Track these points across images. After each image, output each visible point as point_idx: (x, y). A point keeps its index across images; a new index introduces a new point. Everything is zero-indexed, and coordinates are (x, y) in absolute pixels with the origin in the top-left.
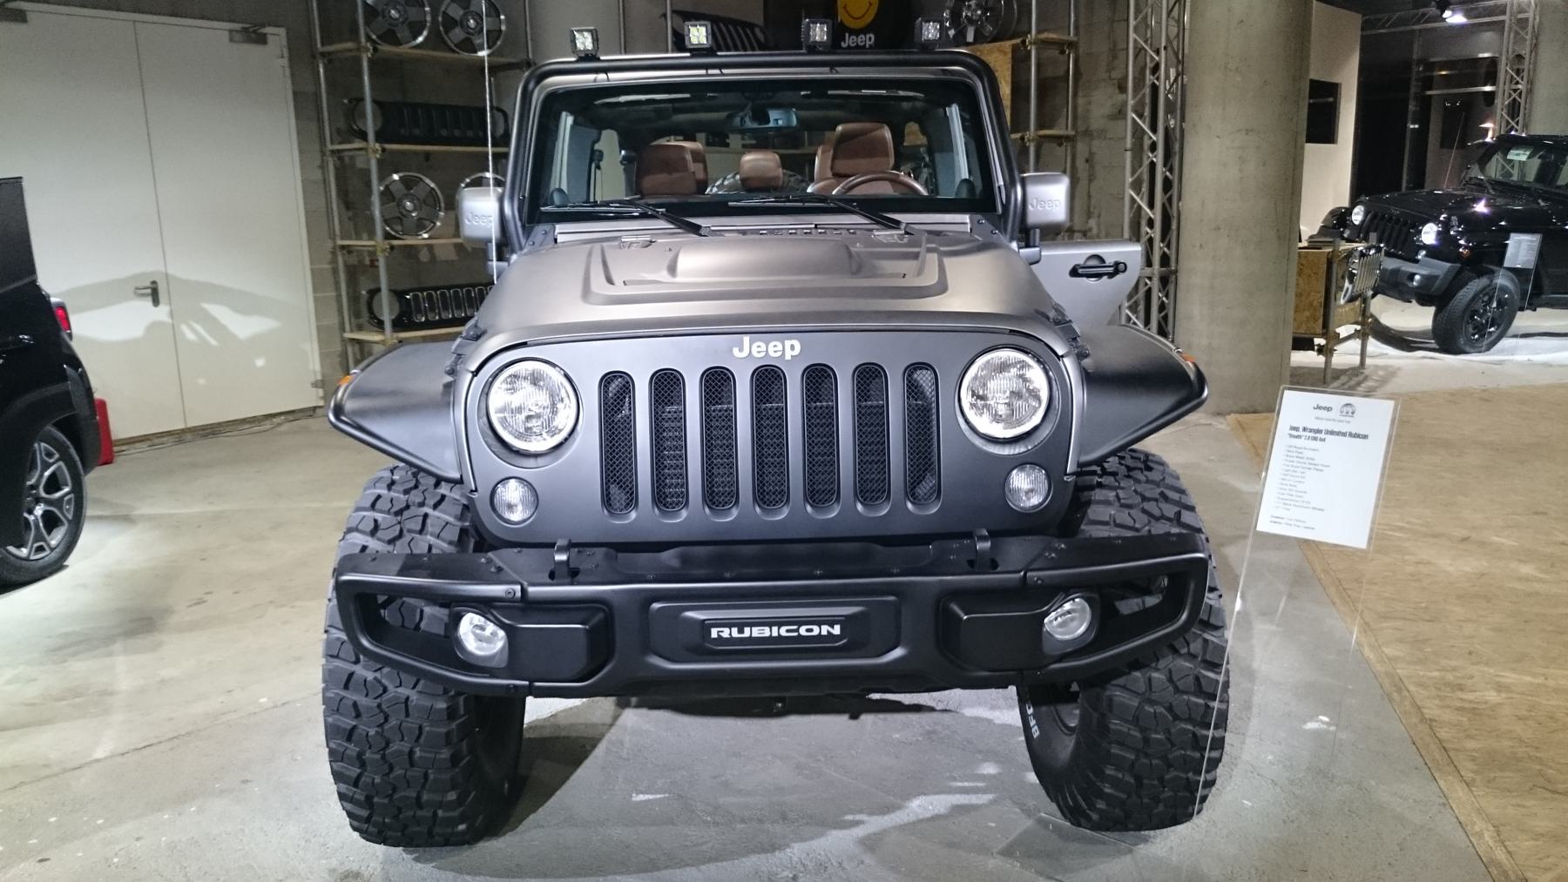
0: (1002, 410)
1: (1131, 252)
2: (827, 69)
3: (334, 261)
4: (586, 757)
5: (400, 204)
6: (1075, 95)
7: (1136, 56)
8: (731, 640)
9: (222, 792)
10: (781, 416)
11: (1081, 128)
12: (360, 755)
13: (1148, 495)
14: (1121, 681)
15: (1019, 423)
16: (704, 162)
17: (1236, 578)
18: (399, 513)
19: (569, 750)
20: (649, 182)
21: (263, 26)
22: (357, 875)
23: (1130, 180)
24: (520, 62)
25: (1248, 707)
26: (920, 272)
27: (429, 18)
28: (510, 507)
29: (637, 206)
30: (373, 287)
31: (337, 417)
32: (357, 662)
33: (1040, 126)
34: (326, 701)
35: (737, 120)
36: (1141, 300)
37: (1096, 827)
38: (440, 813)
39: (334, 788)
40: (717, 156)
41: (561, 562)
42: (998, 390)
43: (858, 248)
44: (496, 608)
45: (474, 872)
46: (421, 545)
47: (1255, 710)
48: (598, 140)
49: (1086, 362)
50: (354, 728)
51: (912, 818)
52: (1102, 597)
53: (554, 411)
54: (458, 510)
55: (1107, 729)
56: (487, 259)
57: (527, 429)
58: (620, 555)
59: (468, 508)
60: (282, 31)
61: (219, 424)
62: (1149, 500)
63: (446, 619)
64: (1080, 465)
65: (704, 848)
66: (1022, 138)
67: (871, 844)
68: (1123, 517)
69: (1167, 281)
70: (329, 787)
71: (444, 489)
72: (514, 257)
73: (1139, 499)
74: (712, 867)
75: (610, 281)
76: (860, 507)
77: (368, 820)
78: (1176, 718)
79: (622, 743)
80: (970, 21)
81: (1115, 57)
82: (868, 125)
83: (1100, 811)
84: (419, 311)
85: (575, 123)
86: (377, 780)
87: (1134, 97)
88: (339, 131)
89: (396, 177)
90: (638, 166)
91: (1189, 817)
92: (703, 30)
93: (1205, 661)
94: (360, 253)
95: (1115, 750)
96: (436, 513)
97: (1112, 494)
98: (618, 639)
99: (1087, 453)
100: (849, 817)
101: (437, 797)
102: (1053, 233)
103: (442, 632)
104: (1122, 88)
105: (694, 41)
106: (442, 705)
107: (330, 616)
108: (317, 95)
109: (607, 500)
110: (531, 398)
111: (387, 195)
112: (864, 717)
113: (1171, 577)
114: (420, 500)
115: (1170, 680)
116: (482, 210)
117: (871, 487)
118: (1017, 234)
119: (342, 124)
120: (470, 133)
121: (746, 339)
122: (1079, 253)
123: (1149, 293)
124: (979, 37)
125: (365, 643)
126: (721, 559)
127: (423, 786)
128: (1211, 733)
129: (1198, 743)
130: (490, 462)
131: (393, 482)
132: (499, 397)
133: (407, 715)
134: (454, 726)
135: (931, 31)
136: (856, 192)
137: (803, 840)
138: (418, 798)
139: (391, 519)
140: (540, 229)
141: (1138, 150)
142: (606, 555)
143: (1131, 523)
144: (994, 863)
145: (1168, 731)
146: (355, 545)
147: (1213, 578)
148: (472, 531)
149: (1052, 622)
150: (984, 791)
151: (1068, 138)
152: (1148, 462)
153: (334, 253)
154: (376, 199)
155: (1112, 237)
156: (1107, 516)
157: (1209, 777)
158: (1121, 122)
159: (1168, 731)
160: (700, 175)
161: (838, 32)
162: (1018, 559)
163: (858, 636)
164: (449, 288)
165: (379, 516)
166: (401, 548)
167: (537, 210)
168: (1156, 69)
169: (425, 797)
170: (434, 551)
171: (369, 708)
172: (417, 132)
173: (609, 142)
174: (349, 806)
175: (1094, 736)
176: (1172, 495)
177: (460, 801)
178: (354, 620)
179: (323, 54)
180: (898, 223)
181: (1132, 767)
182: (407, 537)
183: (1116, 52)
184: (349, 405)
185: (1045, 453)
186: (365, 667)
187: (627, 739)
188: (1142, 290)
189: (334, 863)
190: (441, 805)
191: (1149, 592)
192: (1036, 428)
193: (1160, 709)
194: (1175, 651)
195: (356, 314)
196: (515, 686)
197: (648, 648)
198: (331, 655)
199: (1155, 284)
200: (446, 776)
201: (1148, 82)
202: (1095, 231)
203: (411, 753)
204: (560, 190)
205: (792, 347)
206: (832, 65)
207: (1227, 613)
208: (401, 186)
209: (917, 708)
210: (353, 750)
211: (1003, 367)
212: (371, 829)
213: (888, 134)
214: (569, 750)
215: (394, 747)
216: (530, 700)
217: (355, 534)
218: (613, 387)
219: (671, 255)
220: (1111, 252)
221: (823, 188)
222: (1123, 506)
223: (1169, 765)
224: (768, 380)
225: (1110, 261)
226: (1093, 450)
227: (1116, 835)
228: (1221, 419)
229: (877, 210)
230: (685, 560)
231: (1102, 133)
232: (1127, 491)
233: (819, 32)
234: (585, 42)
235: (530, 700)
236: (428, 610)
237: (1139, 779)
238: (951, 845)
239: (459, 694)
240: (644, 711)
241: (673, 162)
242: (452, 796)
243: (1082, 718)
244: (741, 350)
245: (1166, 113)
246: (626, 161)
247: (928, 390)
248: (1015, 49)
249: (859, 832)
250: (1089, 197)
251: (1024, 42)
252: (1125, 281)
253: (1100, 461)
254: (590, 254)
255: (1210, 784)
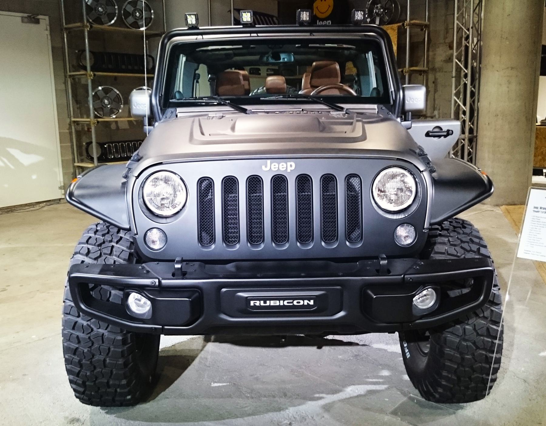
0: (393, 197)
1: (455, 125)
2: (309, 34)
3: (70, 128)
4: (190, 365)
5: (102, 101)
6: (428, 51)
7: (458, 32)
8: (260, 307)
9: (13, 380)
10: (285, 199)
11: (431, 66)
12: (80, 361)
13: (464, 239)
14: (450, 330)
15: (402, 203)
16: (248, 80)
17: (506, 284)
18: (100, 245)
19: (181, 362)
20: (222, 89)
21: (38, 15)
22: (78, 420)
23: (454, 92)
24: (160, 31)
25: (512, 345)
26: (353, 130)
27: (117, 12)
28: (153, 242)
29: (215, 99)
30: (88, 141)
31: (71, 198)
32: (79, 316)
33: (411, 65)
34: (64, 335)
35: (265, 59)
36: (459, 150)
37: (438, 401)
38: (118, 390)
39: (68, 377)
40: (255, 79)
41: (178, 269)
42: (391, 187)
43: (323, 120)
44: (147, 290)
45: (135, 419)
46: (111, 260)
47: (515, 347)
48: (197, 69)
49: (434, 174)
50: (77, 348)
51: (348, 396)
52: (442, 288)
53: (175, 195)
54: (129, 244)
55: (444, 353)
56: (143, 125)
57: (162, 204)
58: (207, 266)
59: (133, 243)
60: (47, 18)
61: (14, 206)
62: (464, 242)
63: (122, 296)
64: (431, 224)
65: (246, 409)
66: (402, 71)
67: (327, 408)
68: (452, 250)
69: (472, 140)
70: (65, 377)
71: (122, 234)
72: (157, 124)
73: (459, 242)
74: (250, 418)
75: (203, 134)
76: (323, 244)
77: (83, 393)
78: (477, 348)
79: (207, 359)
80: (378, 14)
81: (447, 32)
82: (328, 62)
83: (439, 393)
84: (110, 153)
85: (186, 59)
86: (88, 374)
87: (457, 51)
88: (73, 66)
89: (100, 88)
90: (216, 83)
91: (482, 397)
92: (249, 14)
93: (491, 320)
94: (83, 125)
95: (448, 363)
96: (118, 246)
97: (446, 240)
98: (205, 306)
99: (435, 218)
100: (317, 395)
101: (117, 382)
102: (418, 115)
103: (120, 303)
104: (451, 47)
105: (245, 20)
106: (120, 338)
107: (66, 294)
108: (63, 48)
109: (200, 239)
110: (164, 189)
111: (96, 97)
112: (324, 348)
113: (475, 279)
114: (110, 239)
115: (475, 329)
116: (141, 101)
117: (329, 234)
118: (400, 115)
119: (75, 63)
120: (136, 68)
121: (269, 161)
122: (430, 126)
123: (463, 146)
124: (382, 22)
125: (83, 306)
126: (255, 268)
127: (110, 377)
128: (494, 355)
129: (488, 360)
130: (143, 222)
131: (97, 231)
132: (148, 188)
133: (103, 342)
134: (125, 348)
135: (359, 16)
136: (323, 94)
137: (294, 406)
138: (108, 382)
139: (96, 248)
140: (170, 110)
141: (458, 78)
142: (200, 266)
143: (456, 253)
144: (387, 418)
145: (473, 354)
146: (79, 260)
147: (496, 280)
148: (135, 255)
149: (417, 300)
150: (383, 383)
151: (424, 71)
152: (464, 224)
153: (70, 125)
154: (90, 99)
155: (445, 117)
156: (443, 249)
157: (493, 377)
158: (450, 64)
159: (473, 354)
160: (247, 87)
161: (313, 20)
162: (400, 269)
163: (322, 306)
164: (125, 142)
165: (90, 247)
166: (101, 261)
167: (168, 102)
168: (467, 38)
169: (111, 382)
170: (116, 263)
171: (84, 339)
172: (110, 66)
173: (203, 70)
174: (74, 386)
175: (437, 357)
176: (475, 239)
177: (128, 384)
178: (78, 296)
179: (66, 29)
180: (342, 109)
181: (455, 372)
182: (104, 257)
183: (448, 30)
184: (76, 193)
185: (414, 219)
186: (83, 319)
187: (209, 357)
188: (460, 145)
189: (67, 414)
190: (119, 386)
191: (464, 287)
192: (409, 206)
193: (470, 344)
194: (477, 315)
195: (80, 154)
196: (155, 328)
197: (220, 310)
198: (66, 313)
199: (466, 143)
200: (121, 372)
201: (463, 44)
202: (437, 116)
203: (105, 360)
204: (179, 92)
205: (291, 166)
206: (311, 32)
207: (502, 298)
208: (102, 92)
209: (350, 344)
210: (76, 359)
211: (393, 176)
212: (85, 397)
213: (338, 67)
214: (181, 362)
215: (97, 358)
216: (162, 336)
217: (78, 255)
218: (204, 184)
219: (232, 122)
220: (445, 125)
221: (306, 92)
222: (452, 245)
223: (474, 371)
224: (279, 182)
225: (445, 129)
226: (438, 217)
227: (448, 405)
228: (498, 208)
229: (332, 102)
230: (238, 268)
231: (441, 70)
232: (454, 237)
233: (305, 16)
234: (192, 20)
235: (162, 336)
236: (113, 292)
237: (459, 378)
238: (368, 409)
239: (128, 332)
240: (217, 344)
241: (235, 81)
242: (124, 382)
243: (431, 348)
244: (266, 167)
245: (472, 59)
246: (211, 80)
247: (357, 187)
248: (399, 28)
249: (321, 402)
250: (434, 100)
251: (403, 24)
252: (452, 140)
253: (440, 223)
254: (193, 122)
255: (494, 380)
